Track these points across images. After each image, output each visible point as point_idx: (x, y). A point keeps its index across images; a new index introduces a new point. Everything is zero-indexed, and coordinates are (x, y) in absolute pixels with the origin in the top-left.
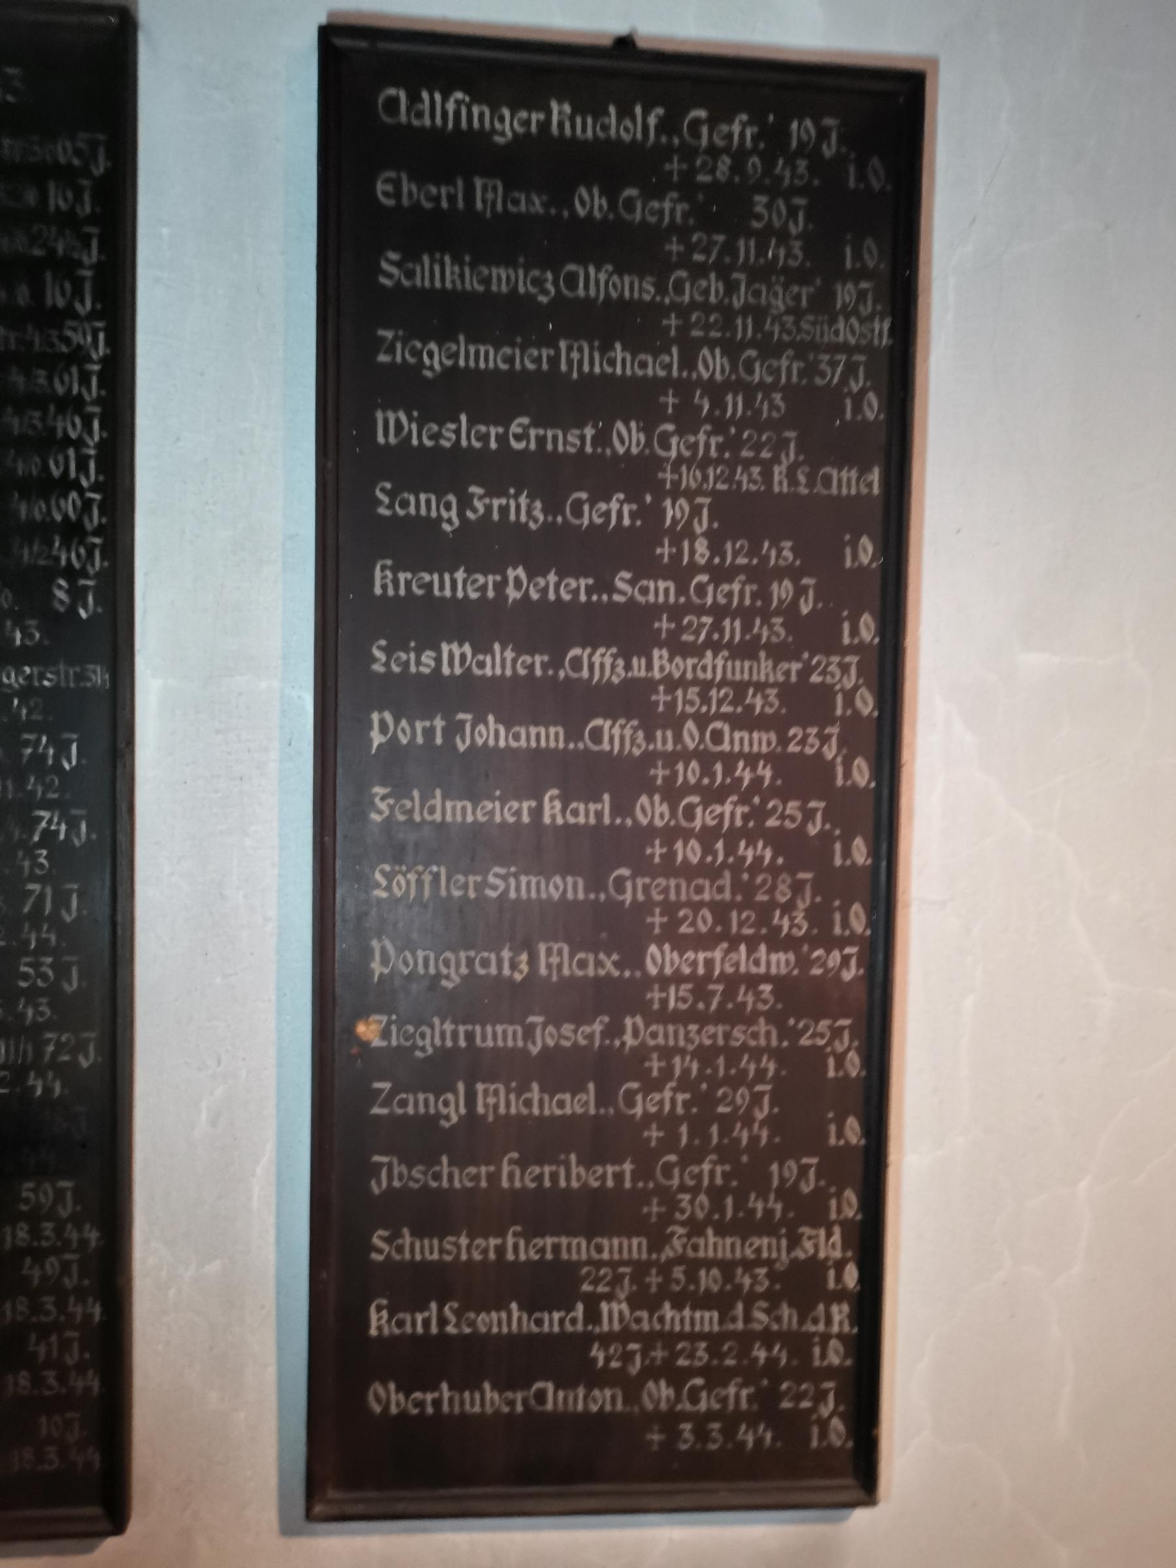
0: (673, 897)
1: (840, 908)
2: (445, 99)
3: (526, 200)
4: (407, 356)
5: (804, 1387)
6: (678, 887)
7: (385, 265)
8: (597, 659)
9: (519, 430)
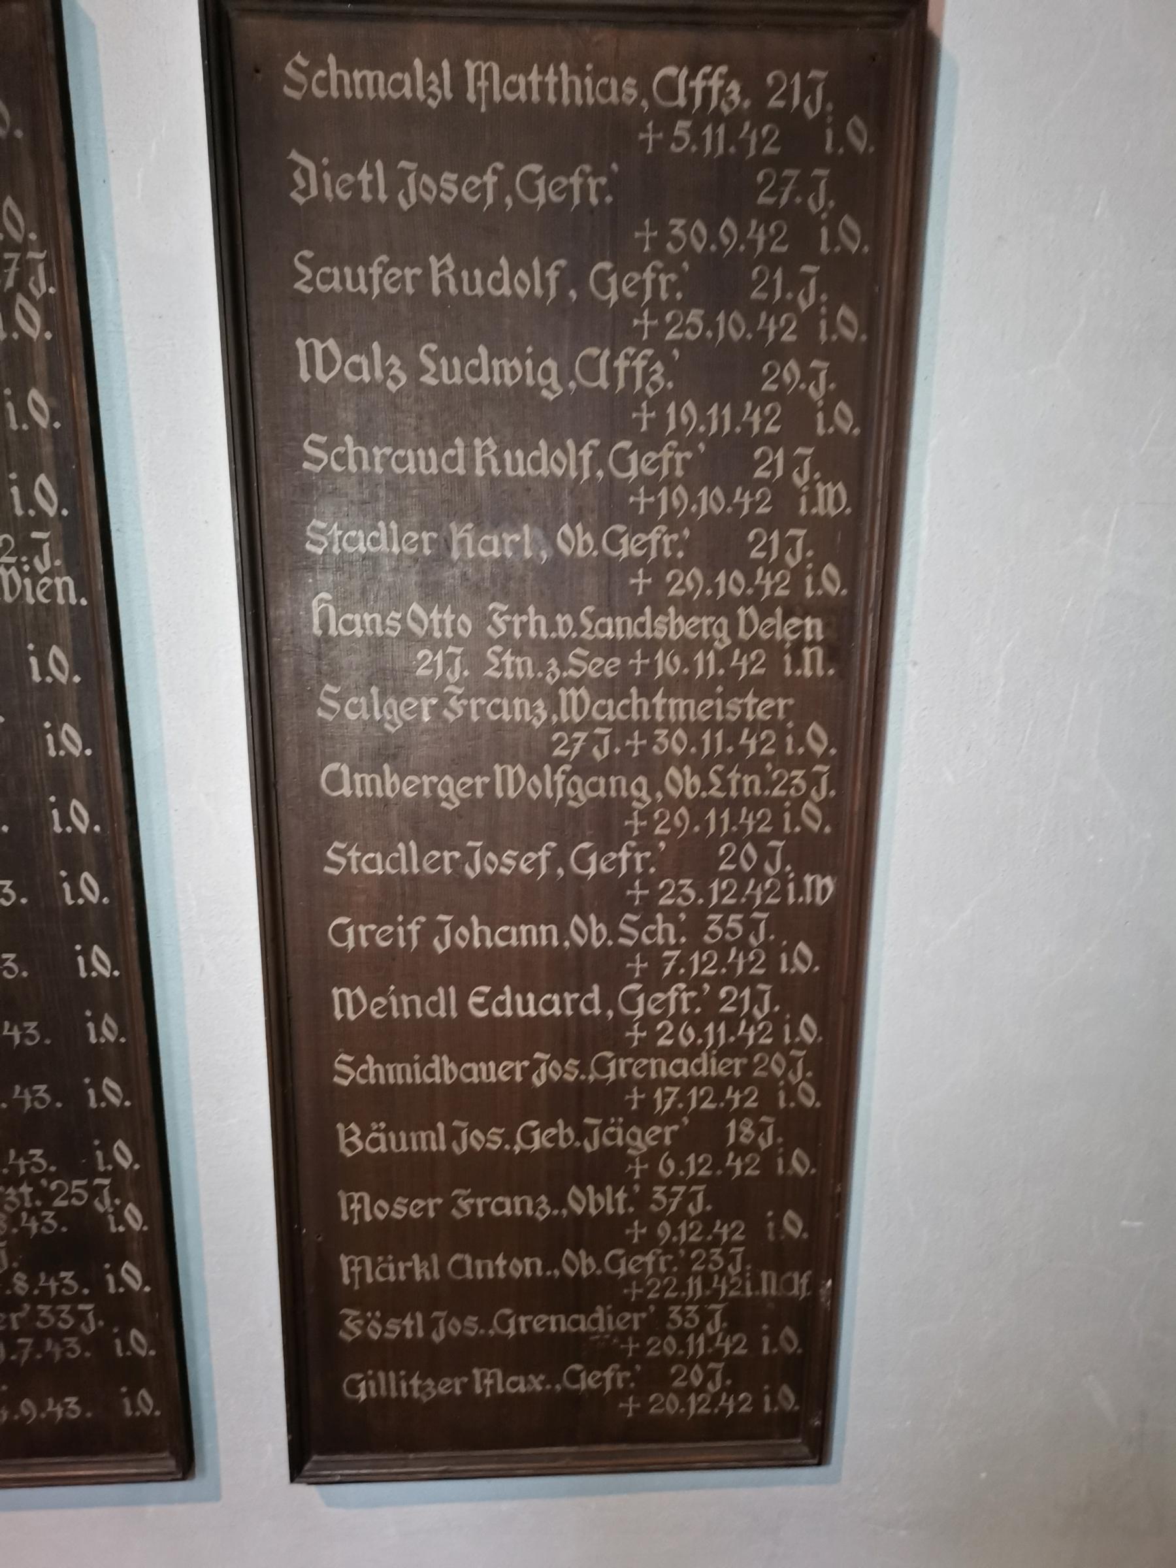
0: (653, 1075)
1: (769, 1392)
2: (579, 447)
3: (470, 710)
4: (339, 191)
5: (742, 1396)
6: (658, 1066)
7: (289, 70)
8: (621, 364)
9: (481, 1000)
